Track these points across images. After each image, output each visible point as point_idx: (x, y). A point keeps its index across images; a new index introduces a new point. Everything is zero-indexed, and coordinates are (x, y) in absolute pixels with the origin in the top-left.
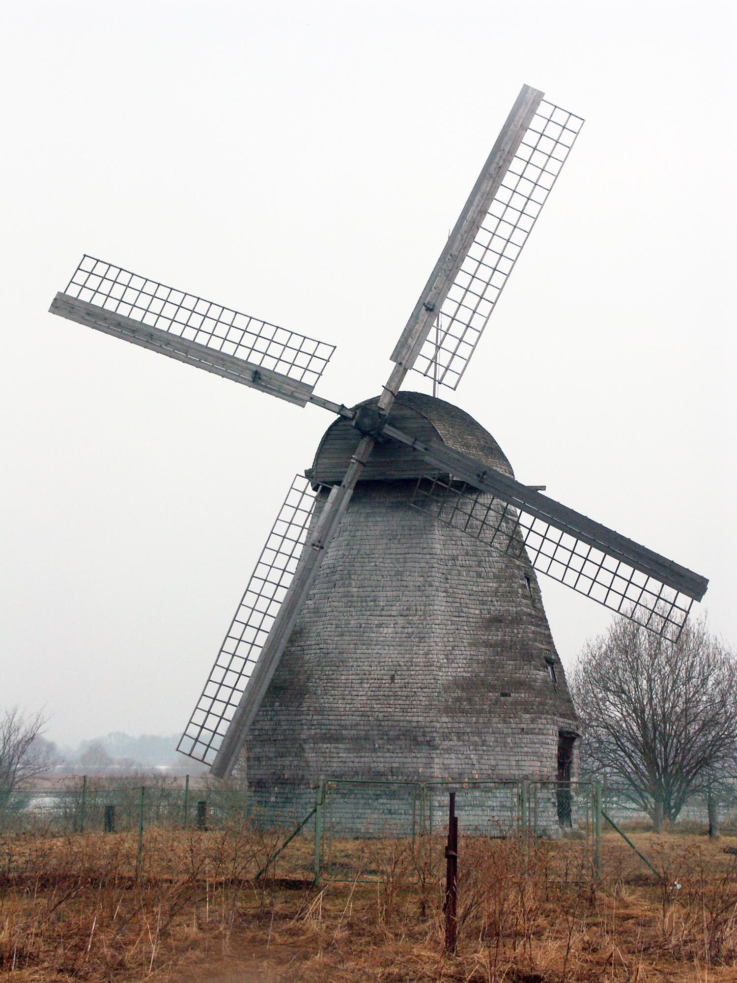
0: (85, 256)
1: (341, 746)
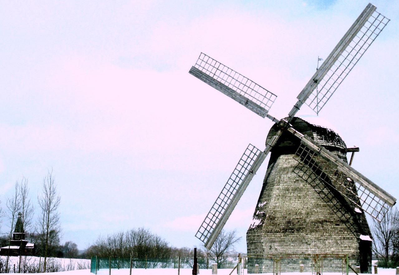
1: (275, 244)
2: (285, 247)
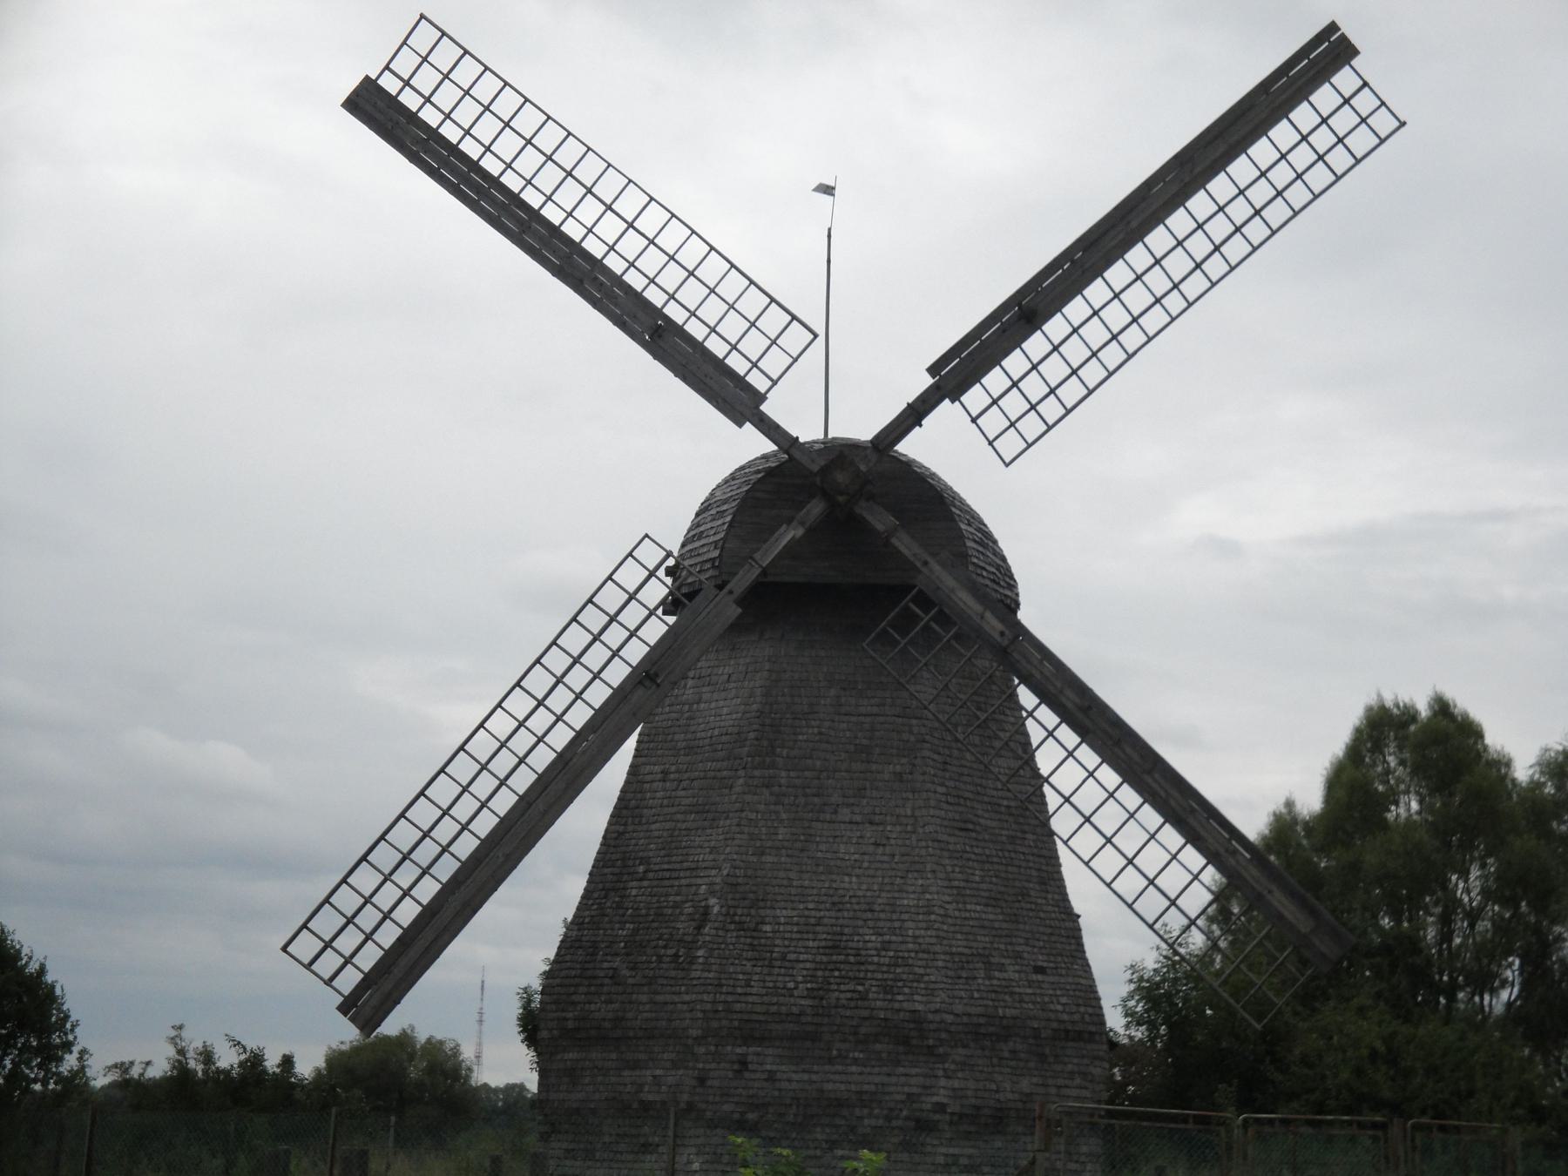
0: (422, 17)
2: (815, 1068)
